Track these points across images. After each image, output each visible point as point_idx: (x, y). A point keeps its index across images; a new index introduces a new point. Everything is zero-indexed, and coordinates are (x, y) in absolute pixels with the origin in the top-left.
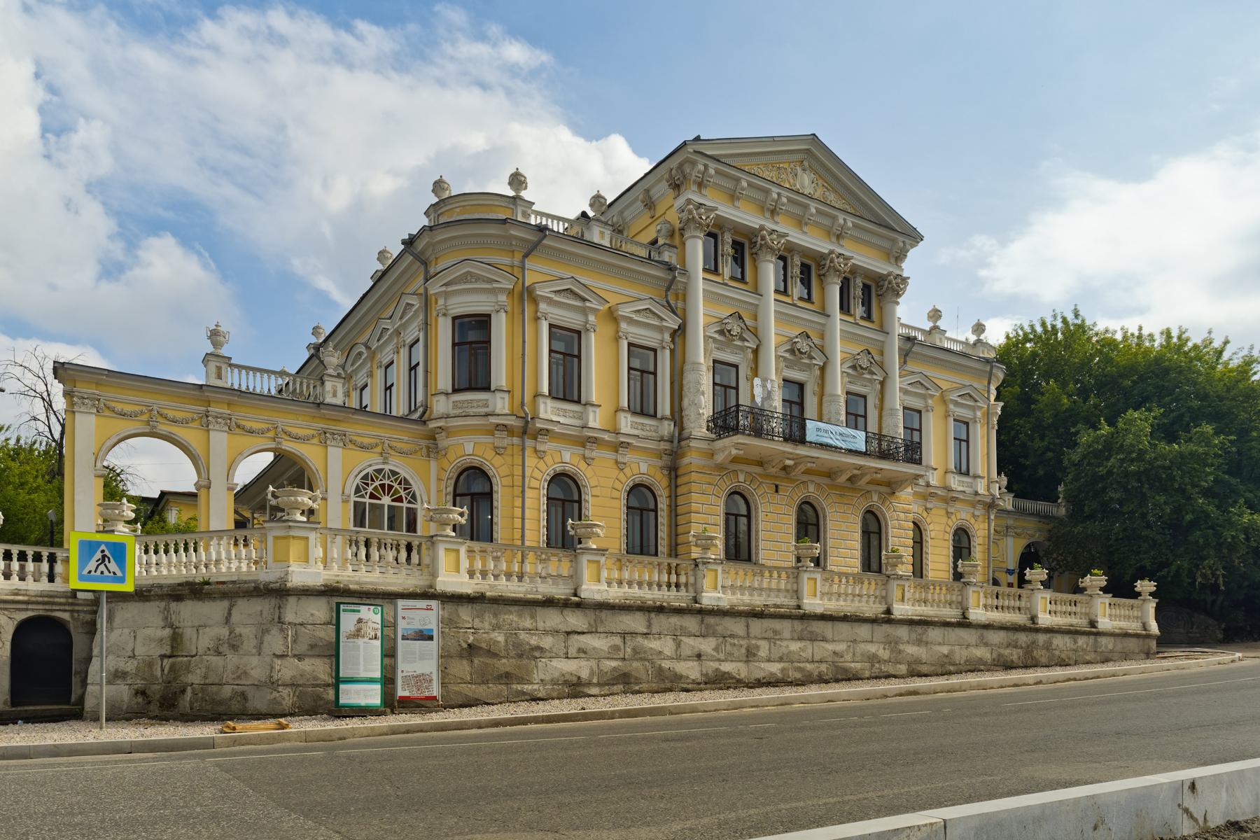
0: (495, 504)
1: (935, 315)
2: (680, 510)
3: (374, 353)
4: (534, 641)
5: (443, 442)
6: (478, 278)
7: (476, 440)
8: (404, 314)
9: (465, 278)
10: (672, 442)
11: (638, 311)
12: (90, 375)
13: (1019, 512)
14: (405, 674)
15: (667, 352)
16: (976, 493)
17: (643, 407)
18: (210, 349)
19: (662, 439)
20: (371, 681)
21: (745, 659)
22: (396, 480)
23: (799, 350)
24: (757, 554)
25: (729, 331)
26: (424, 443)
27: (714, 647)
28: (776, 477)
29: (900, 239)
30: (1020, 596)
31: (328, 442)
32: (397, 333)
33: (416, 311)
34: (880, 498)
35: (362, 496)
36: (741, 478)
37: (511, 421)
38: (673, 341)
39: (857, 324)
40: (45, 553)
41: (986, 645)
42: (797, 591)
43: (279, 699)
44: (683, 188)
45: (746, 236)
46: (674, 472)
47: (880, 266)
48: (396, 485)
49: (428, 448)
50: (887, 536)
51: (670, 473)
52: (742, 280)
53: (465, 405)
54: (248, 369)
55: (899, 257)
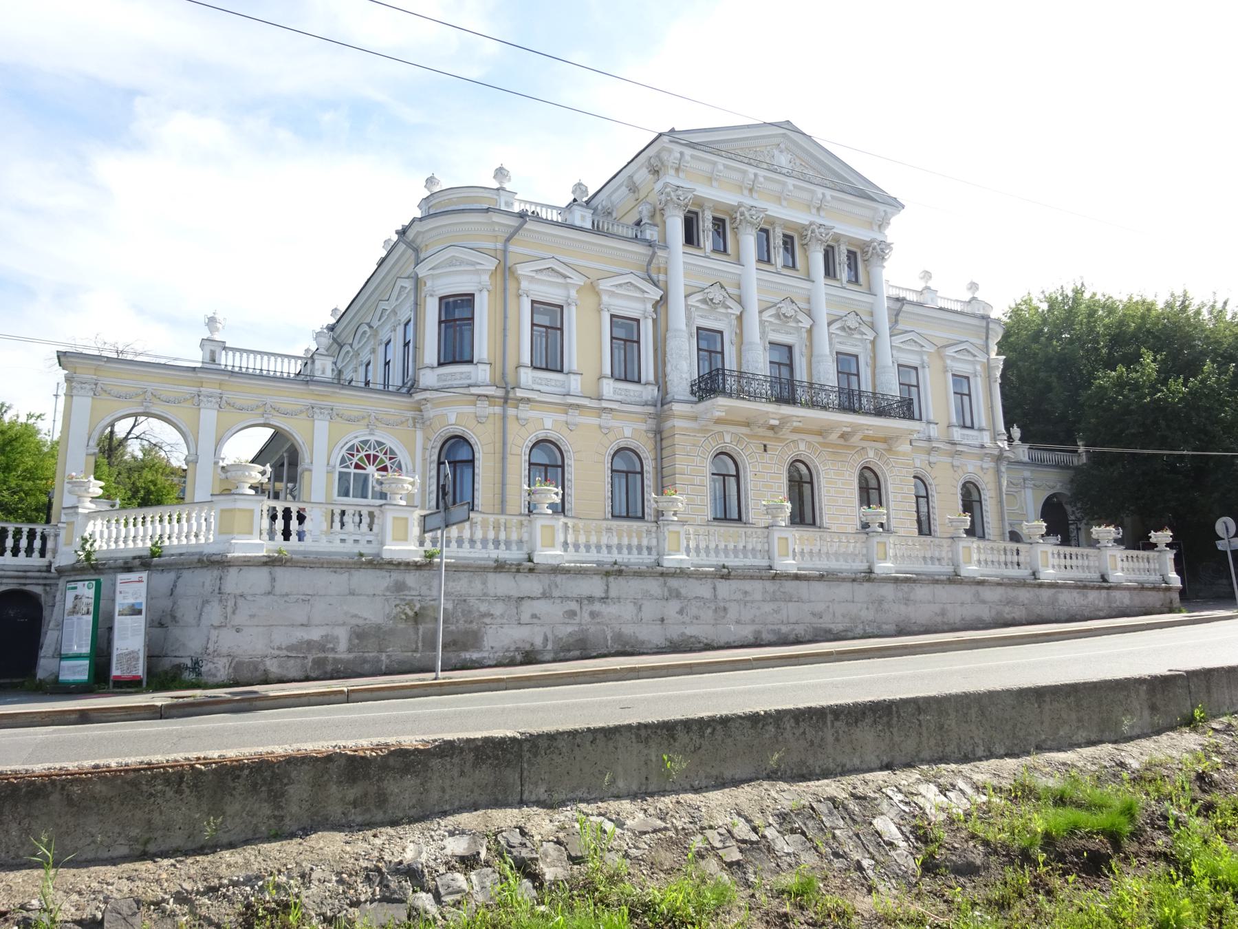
0: (476, 471)
1: (500, 173)
2: (666, 472)
3: (376, 331)
4: (483, 608)
5: (430, 413)
6: (462, 262)
7: (459, 411)
8: (399, 294)
9: (452, 262)
10: (655, 406)
11: (620, 285)
12: (137, 368)
13: (1034, 463)
14: (119, 652)
15: (650, 322)
16: (982, 447)
17: (627, 373)
18: (207, 335)
19: (646, 404)
20: (78, 657)
21: (713, 622)
22: (381, 450)
23: (784, 314)
24: (747, 513)
25: (711, 300)
26: (410, 414)
27: (678, 610)
28: (764, 437)
29: (882, 208)
30: (1018, 550)
31: (315, 416)
32: (394, 312)
33: (408, 293)
34: (876, 454)
35: (347, 467)
36: (728, 438)
37: (491, 391)
38: (655, 311)
39: (844, 288)
40: (25, 528)
41: (984, 602)
42: (768, 551)
43: (213, 671)
44: (661, 173)
45: (726, 213)
46: (659, 435)
47: (864, 234)
48: (381, 455)
49: (414, 419)
50: (887, 492)
51: (655, 436)
52: (857, 281)
53: (449, 377)
54: (241, 351)
55: (882, 224)
